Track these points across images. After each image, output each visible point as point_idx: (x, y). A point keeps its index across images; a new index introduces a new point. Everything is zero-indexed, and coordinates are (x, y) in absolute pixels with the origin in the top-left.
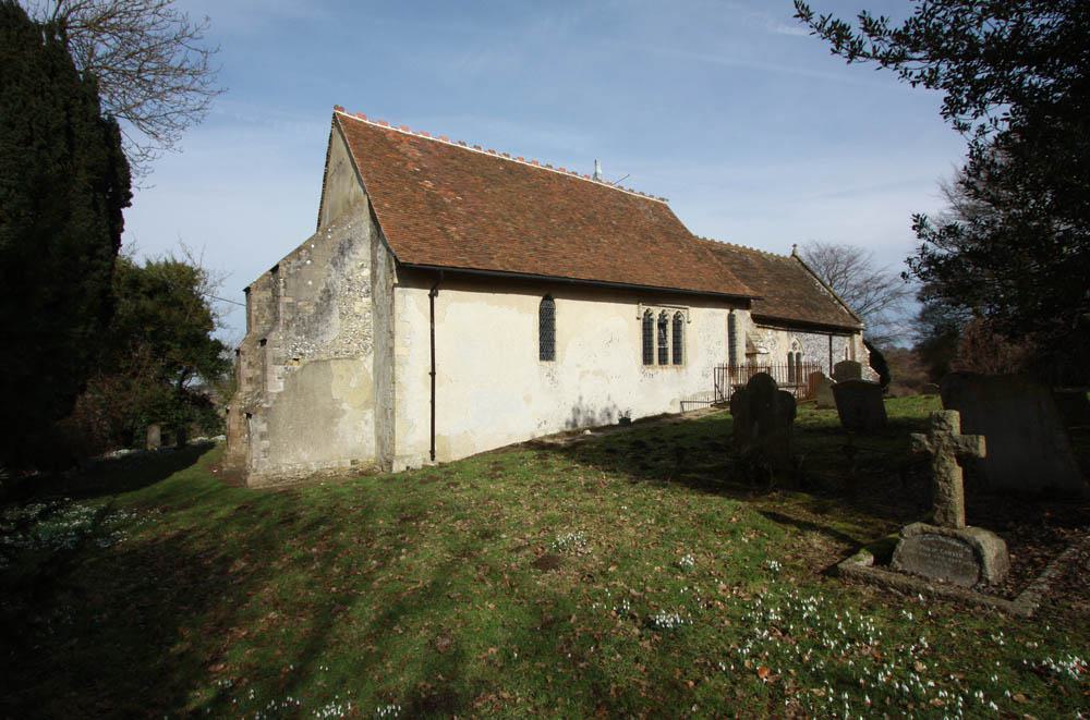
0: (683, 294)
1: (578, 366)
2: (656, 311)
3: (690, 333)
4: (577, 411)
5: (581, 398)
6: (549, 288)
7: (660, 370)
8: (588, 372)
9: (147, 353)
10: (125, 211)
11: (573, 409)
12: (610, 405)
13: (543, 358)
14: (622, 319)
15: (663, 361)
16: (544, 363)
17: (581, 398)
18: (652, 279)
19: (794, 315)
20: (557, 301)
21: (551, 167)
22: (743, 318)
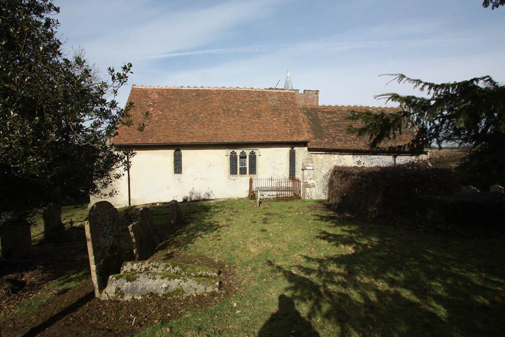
0: (182, 145)
1: (192, 176)
2: (238, 152)
3: (260, 161)
4: (192, 193)
5: (193, 189)
6: (292, 144)
7: (240, 178)
8: (197, 178)
9: (283, 247)
10: (435, 84)
11: (190, 193)
12: (210, 191)
13: (176, 172)
14: (221, 157)
15: (243, 172)
16: (176, 175)
17: (193, 189)
18: (234, 140)
19: (327, 147)
20: (182, 151)
21: (224, 88)
22: (301, 153)
